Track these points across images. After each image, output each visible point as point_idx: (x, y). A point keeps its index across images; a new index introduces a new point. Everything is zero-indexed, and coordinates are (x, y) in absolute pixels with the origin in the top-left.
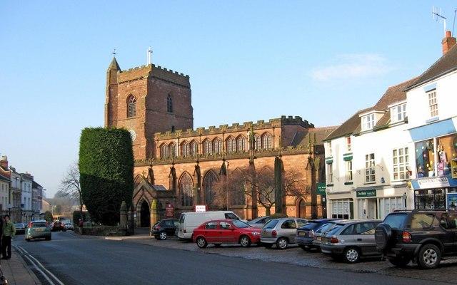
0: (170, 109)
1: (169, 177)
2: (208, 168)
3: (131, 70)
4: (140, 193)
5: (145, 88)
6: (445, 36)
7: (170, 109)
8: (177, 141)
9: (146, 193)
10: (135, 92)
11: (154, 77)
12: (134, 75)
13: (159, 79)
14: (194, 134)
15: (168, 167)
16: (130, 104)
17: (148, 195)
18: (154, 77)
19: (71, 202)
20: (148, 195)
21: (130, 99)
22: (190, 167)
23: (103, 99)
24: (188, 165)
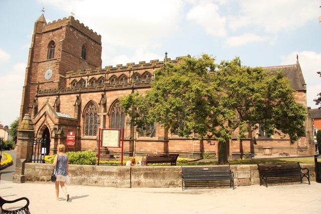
0: (84, 56)
1: (75, 105)
2: (114, 99)
3: (54, 22)
4: (42, 119)
5: (63, 35)
6: (235, 58)
7: (84, 56)
8: (86, 78)
9: (48, 119)
10: (55, 39)
11: (72, 27)
12: (56, 28)
13: (77, 30)
14: (103, 72)
15: (74, 97)
16: (131, 150)
17: (50, 122)
18: (72, 27)
19: (66, 135)
20: (50, 122)
21: (52, 44)
22: (96, 97)
23: (29, 45)
24: (95, 94)
